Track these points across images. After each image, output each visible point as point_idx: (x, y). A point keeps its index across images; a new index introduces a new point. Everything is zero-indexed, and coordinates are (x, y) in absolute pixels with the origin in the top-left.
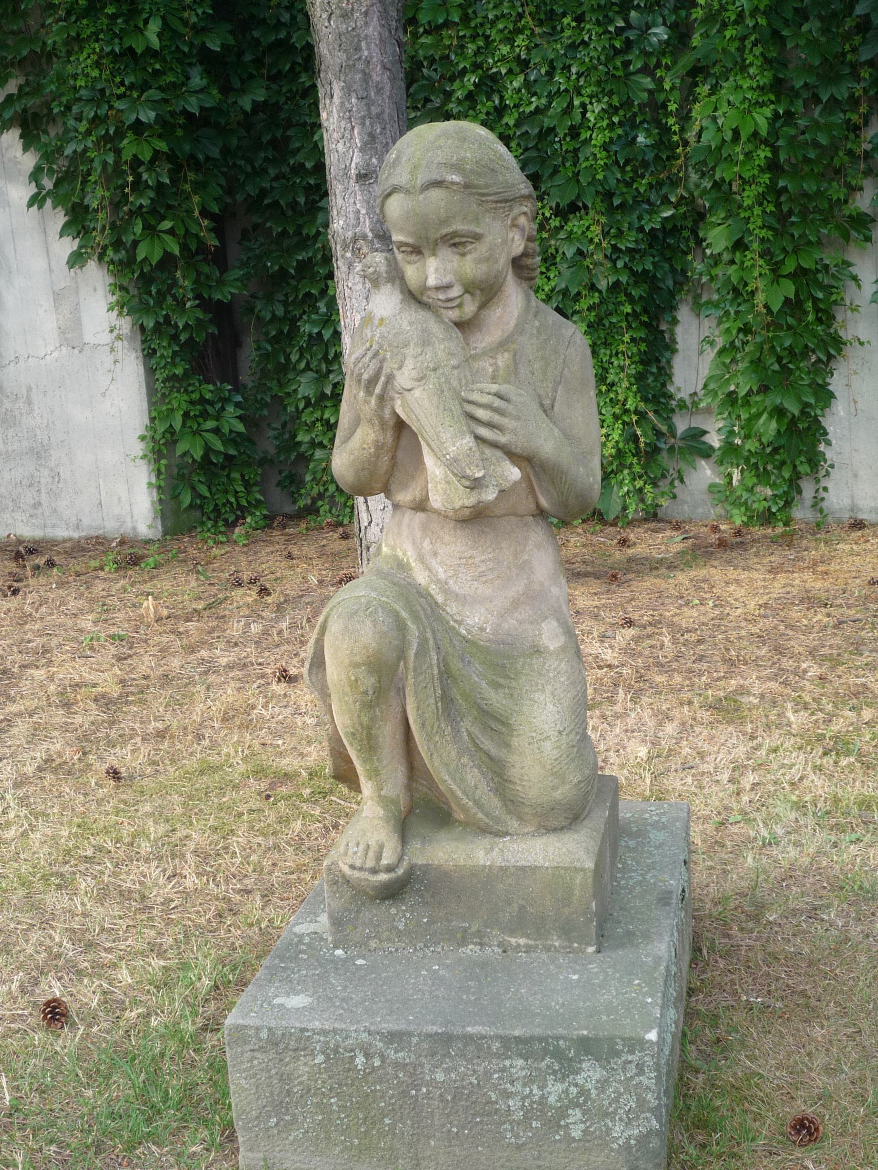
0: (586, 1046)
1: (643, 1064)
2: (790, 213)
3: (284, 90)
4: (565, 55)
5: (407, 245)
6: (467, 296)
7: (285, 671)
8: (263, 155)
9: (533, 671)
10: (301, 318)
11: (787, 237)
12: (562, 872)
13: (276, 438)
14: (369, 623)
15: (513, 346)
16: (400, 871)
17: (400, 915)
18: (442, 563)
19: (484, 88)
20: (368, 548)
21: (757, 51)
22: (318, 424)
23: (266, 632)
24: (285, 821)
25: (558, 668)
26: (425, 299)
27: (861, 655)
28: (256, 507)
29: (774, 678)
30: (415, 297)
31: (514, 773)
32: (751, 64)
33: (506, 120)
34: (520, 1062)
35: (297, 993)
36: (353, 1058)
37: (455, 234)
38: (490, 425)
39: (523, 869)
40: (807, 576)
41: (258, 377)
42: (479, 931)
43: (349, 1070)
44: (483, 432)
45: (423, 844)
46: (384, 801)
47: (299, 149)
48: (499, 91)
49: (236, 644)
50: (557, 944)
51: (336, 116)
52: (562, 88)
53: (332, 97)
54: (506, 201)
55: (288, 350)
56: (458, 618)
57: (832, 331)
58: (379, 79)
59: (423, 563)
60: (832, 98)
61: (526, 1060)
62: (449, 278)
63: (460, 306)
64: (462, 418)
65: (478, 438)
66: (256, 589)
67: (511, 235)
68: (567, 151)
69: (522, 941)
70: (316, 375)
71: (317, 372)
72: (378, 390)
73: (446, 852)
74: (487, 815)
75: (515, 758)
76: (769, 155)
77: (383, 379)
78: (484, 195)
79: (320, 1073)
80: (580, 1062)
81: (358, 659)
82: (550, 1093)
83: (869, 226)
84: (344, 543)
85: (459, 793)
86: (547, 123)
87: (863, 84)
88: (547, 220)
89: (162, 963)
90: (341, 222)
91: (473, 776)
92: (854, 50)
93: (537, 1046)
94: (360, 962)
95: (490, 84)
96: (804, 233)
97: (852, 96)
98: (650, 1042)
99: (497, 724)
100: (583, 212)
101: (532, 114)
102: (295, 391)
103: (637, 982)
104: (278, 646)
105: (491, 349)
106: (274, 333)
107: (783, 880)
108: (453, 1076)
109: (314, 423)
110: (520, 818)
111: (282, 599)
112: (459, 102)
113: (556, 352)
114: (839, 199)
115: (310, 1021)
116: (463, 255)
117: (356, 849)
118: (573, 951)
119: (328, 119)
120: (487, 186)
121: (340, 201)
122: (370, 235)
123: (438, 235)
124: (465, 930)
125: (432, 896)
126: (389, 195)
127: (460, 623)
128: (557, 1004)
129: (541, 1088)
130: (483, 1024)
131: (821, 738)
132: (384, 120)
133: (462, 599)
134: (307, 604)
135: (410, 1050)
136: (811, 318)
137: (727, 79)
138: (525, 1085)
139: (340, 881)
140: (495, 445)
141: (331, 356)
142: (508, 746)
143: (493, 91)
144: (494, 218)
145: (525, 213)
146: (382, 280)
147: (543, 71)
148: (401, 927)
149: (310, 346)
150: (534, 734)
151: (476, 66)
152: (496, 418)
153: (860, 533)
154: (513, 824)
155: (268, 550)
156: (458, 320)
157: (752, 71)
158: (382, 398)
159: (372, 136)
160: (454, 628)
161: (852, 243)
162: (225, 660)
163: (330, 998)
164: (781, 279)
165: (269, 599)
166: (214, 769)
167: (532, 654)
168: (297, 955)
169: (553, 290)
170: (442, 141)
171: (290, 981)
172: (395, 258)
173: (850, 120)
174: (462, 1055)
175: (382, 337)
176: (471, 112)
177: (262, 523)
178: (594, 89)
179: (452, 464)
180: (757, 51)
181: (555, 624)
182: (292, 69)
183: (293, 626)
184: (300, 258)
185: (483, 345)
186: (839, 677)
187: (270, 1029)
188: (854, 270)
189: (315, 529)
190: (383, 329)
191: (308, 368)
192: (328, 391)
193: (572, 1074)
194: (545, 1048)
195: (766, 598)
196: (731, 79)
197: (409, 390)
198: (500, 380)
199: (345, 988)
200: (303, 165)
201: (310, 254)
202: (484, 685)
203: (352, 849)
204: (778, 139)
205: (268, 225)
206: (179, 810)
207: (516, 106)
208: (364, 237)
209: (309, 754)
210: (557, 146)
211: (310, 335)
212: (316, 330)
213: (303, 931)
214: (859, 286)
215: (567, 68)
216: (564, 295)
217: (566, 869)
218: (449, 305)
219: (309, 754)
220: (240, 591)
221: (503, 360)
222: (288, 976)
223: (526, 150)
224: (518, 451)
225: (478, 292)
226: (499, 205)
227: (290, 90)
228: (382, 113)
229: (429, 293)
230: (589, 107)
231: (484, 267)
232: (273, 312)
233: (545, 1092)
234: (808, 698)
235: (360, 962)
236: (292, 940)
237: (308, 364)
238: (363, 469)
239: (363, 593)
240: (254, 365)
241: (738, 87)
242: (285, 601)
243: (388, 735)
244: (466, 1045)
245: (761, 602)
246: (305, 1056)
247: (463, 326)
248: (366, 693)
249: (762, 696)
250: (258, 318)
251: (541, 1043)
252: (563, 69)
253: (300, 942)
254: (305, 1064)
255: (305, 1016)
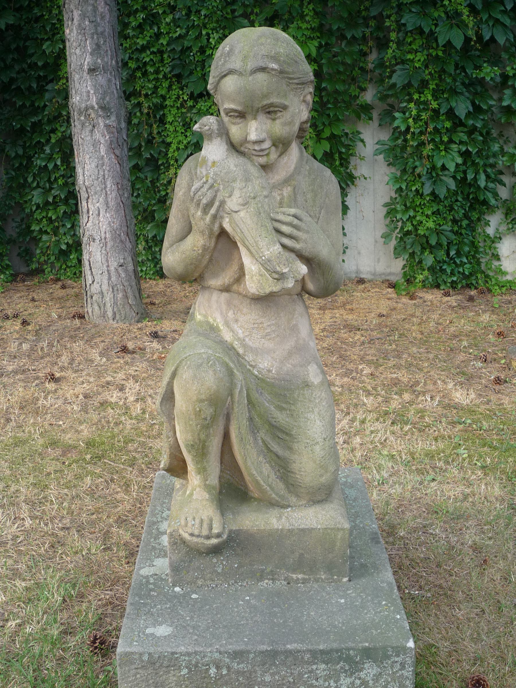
0: (368, 654)
1: (405, 663)
2: (328, 102)
3: (24, 17)
4: (197, 4)
5: (235, 111)
6: (273, 148)
7: (53, 375)
8: (11, 56)
9: (305, 399)
10: (34, 156)
11: (325, 116)
12: (329, 531)
13: (17, 227)
14: (211, 372)
15: (293, 182)
16: (225, 537)
17: (219, 563)
18: (241, 327)
19: (148, 21)
20: (92, 297)
21: (311, 7)
22: (44, 220)
23: (32, 349)
24: (79, 477)
25: (321, 395)
26: (242, 149)
27: (389, 360)
28: (6, 269)
29: (346, 375)
30: (235, 148)
31: (295, 467)
32: (307, 15)
33: (161, 41)
34: (323, 666)
35: (160, 624)
36: (207, 670)
37: (271, 105)
38: (290, 237)
39: (303, 530)
40: (342, 311)
41: (6, 190)
42: (272, 571)
43: (205, 677)
44: (286, 241)
45: (234, 514)
46: (208, 488)
47: (33, 54)
48: (157, 24)
49: (15, 357)
50: (323, 577)
51: (75, 32)
52: (196, 23)
53: (73, 20)
54: (303, 84)
55: (26, 175)
56: (253, 363)
57: (349, 171)
58: (102, 10)
59: (228, 327)
60: (353, 37)
61: (327, 664)
62: (264, 135)
63: (267, 155)
64: (273, 231)
65: (284, 246)
66: (20, 321)
67: (302, 108)
68: (198, 61)
69: (300, 576)
70: (43, 191)
71: (43, 189)
72: (213, 211)
73: (252, 520)
74: (277, 494)
75: (296, 456)
76: (317, 68)
77: (217, 204)
78: (291, 79)
79: (184, 681)
80: (363, 664)
81: (203, 397)
82: (341, 685)
83: (371, 111)
84: (64, 291)
85: (262, 482)
86: (186, 44)
87: (370, 30)
88: (185, 101)
89: (23, 584)
90: (78, 98)
91: (266, 469)
92: (367, 9)
93: (335, 655)
94: (194, 596)
95: (152, 19)
96: (336, 114)
97: (364, 35)
98: (410, 648)
99: (282, 434)
100: (206, 97)
101: (177, 38)
102: (31, 200)
103: (384, 603)
104: (42, 358)
105: (279, 184)
106: (17, 165)
107: (398, 507)
108: (277, 677)
109: (42, 219)
110: (297, 496)
111: (38, 328)
112: (133, 29)
113: (321, 187)
114: (355, 95)
115: (178, 646)
116: (274, 120)
117: (193, 522)
118: (334, 581)
119: (70, 34)
120: (293, 73)
121: (77, 85)
122: (96, 106)
123: (260, 105)
124: (263, 571)
125: (242, 550)
126: (225, 76)
127: (254, 367)
128: (339, 623)
129: (336, 682)
130: (296, 642)
131: (386, 413)
132: (105, 36)
133: (256, 351)
134: (54, 331)
135: (248, 663)
136: (337, 163)
137: (293, 23)
138: (325, 681)
139: (178, 542)
140: (291, 250)
141: (52, 179)
142: (290, 449)
143: (153, 23)
144: (295, 95)
145: (311, 93)
146: (214, 135)
147: (184, 13)
148: (220, 570)
149: (40, 173)
150: (308, 441)
151: (144, 8)
152: (295, 232)
153: (363, 286)
154: (293, 500)
155: (18, 295)
156: (265, 164)
157: (308, 18)
158: (215, 217)
159: (98, 46)
160: (250, 370)
161: (361, 121)
162: (11, 367)
163: (184, 627)
164: (322, 141)
165: (30, 328)
166: (24, 442)
167: (303, 387)
168: (149, 593)
169: (189, 143)
170: (263, 40)
171: (152, 614)
172: (222, 120)
173: (362, 49)
174: (284, 663)
175: (216, 174)
176: (141, 36)
177: (10, 279)
178: (215, 25)
179: (266, 265)
180: (311, 7)
181: (315, 366)
182: (29, 5)
183: (51, 345)
184: (33, 120)
185: (273, 181)
186: (381, 373)
187: (150, 654)
188: (362, 136)
189: (44, 282)
190: (216, 169)
191: (38, 186)
192: (51, 200)
193: (357, 671)
194: (340, 656)
195: (324, 325)
196: (295, 23)
197: (236, 212)
198: (285, 205)
199: (192, 618)
200: (36, 64)
201: (40, 118)
202: (273, 408)
203: (191, 523)
204: (322, 59)
205: (14, 100)
206: (8, 472)
207: (168, 33)
208: (93, 108)
209: (82, 431)
210: (192, 58)
211: (40, 167)
212: (44, 164)
213: (147, 573)
214: (365, 146)
215: (198, 12)
216: (195, 146)
217: (332, 529)
218: (261, 153)
219: (82, 431)
220: (9, 323)
221: (287, 191)
222: (149, 611)
223: (173, 60)
224: (307, 254)
225: (281, 145)
226: (299, 86)
227: (28, 18)
228: (105, 31)
229: (247, 145)
230: (211, 36)
231: (287, 128)
232: (16, 152)
233: (338, 684)
234: (369, 388)
235: (194, 596)
236: (141, 581)
237: (38, 183)
238: (191, 264)
239: (203, 351)
240: (4, 184)
241: (299, 28)
242: (40, 329)
243: (215, 444)
244: (286, 657)
245: (321, 327)
246: (174, 670)
247: (265, 168)
248: (205, 419)
249: (342, 386)
250: (7, 156)
251: (337, 653)
252: (196, 12)
253: (148, 582)
254: (174, 675)
255: (173, 643)
